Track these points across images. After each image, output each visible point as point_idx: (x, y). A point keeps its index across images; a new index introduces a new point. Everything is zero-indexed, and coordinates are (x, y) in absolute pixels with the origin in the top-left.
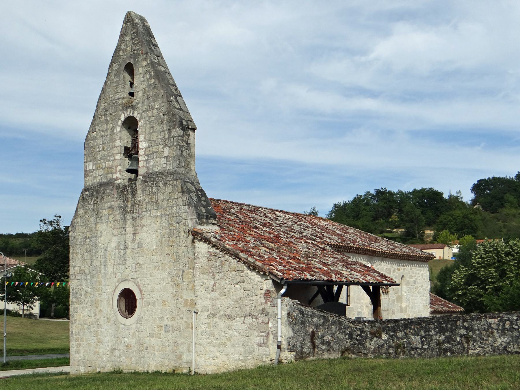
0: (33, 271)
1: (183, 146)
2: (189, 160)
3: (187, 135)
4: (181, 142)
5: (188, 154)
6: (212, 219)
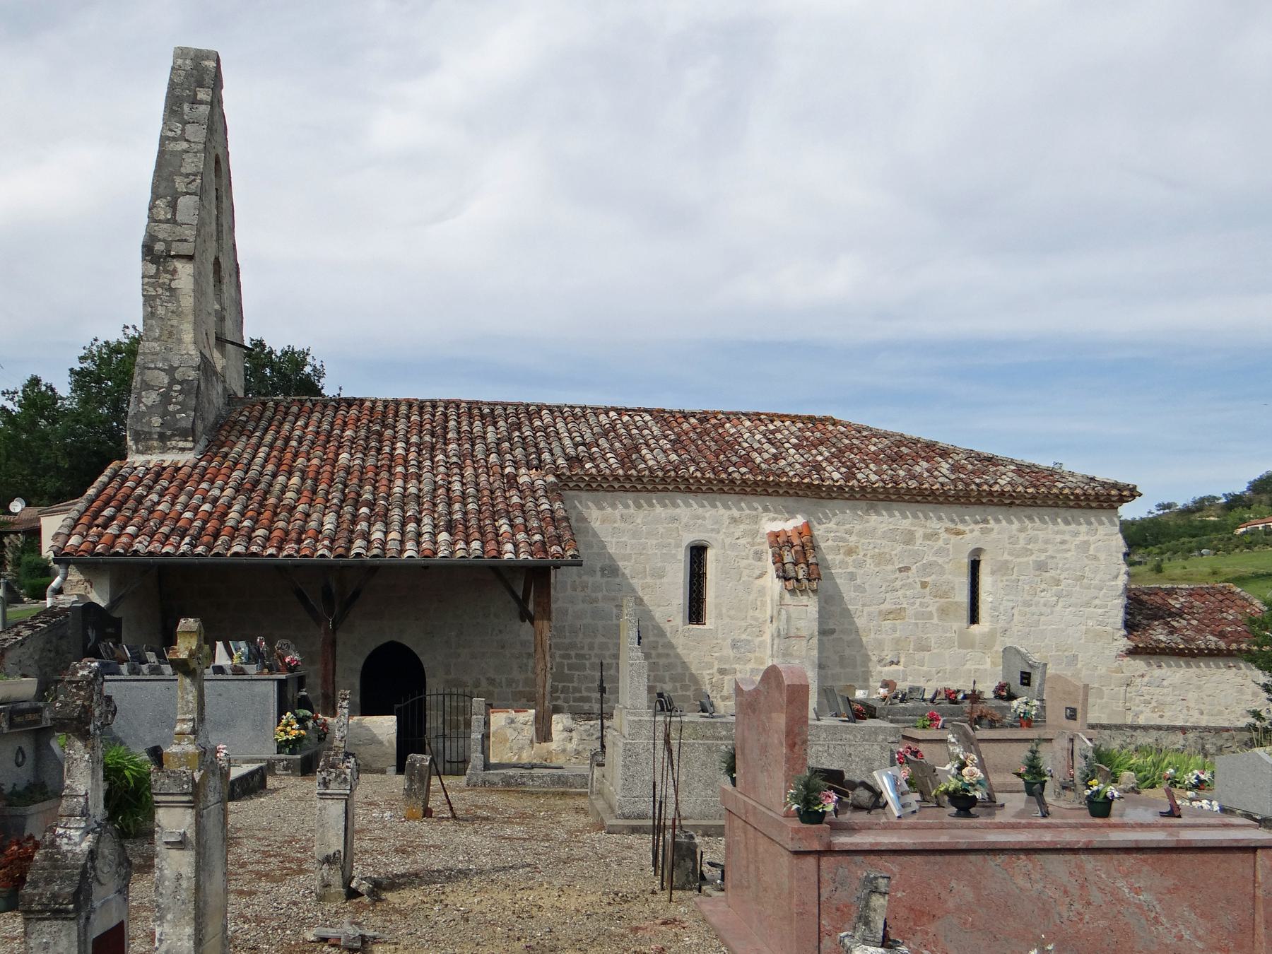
0: (1212, 518)
1: (157, 296)
2: (175, 323)
3: (167, 272)
4: (151, 289)
5: (173, 312)
6: (177, 438)
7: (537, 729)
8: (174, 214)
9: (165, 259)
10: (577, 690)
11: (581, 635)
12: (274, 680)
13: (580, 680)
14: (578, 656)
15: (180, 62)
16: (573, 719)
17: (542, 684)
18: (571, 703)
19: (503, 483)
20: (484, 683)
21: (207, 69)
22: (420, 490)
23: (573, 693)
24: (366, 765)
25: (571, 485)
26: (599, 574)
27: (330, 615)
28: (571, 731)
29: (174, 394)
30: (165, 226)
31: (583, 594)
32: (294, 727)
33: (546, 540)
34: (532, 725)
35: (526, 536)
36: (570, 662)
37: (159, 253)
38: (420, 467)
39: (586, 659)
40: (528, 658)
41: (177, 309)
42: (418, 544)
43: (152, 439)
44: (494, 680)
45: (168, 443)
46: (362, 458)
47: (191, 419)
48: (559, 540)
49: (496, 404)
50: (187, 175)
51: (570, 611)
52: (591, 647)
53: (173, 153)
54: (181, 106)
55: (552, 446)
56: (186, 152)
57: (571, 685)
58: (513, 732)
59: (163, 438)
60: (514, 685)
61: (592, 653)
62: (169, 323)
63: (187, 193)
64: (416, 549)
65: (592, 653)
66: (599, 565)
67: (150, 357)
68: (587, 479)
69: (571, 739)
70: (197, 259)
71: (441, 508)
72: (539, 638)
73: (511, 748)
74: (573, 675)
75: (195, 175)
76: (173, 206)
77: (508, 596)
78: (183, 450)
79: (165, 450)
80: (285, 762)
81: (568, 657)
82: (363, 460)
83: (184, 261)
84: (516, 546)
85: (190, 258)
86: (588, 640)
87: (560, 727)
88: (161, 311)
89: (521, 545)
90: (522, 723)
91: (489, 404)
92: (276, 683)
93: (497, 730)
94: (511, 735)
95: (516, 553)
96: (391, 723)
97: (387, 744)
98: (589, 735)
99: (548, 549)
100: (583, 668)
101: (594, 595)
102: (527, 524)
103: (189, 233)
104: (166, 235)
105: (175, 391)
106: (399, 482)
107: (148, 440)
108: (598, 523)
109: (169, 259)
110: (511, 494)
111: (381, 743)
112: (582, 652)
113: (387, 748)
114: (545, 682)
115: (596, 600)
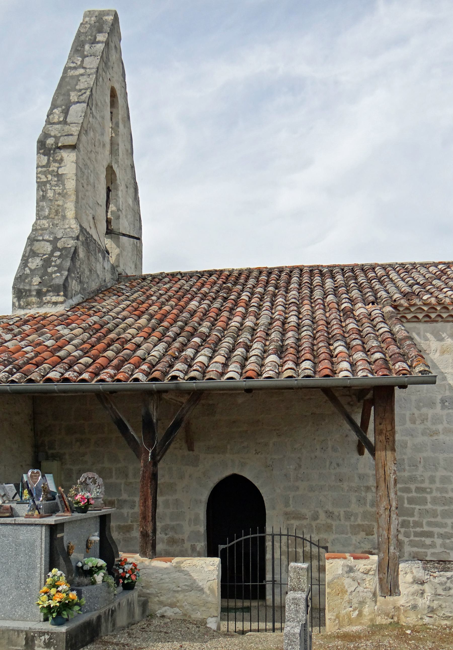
1: (48, 182)
2: (60, 203)
3: (55, 161)
5: (59, 194)
6: (51, 294)
7: (381, 580)
8: (66, 117)
9: (54, 151)
10: (417, 524)
11: (421, 469)
12: (42, 525)
13: (421, 514)
14: (419, 490)
15: (87, 19)
16: (425, 569)
17: (386, 526)
18: (412, 538)
19: (340, 316)
20: (322, 516)
21: (107, 21)
22: (256, 324)
23: (414, 527)
24: (185, 615)
25: (409, 316)
26: (439, 406)
27: (150, 446)
28: (423, 583)
29: (54, 259)
30: (57, 126)
31: (422, 426)
32: (60, 589)
33: (388, 359)
34: (374, 575)
35: (364, 355)
36: (410, 495)
37: (50, 146)
38: (260, 307)
39: (428, 493)
40: (366, 492)
41: (63, 191)
42: (243, 366)
43: (31, 296)
44: (332, 513)
45: (44, 298)
46: (209, 305)
47: (64, 277)
48: (404, 357)
49: (334, 266)
50: (80, 90)
51: (409, 444)
52: (432, 480)
53: (72, 77)
54: (83, 46)
55: (387, 288)
56: (82, 75)
57: (411, 519)
58: (352, 583)
59: (40, 294)
60: (352, 518)
61: (433, 486)
62: (56, 203)
63: (78, 102)
64: (240, 371)
65: (433, 486)
66: (439, 397)
67: (40, 232)
68: (426, 308)
69: (422, 594)
70: (82, 148)
71: (275, 336)
72: (381, 471)
73: (350, 602)
74: (414, 509)
75: (86, 89)
76: (66, 112)
77: (347, 426)
78: (55, 303)
79: (41, 304)
80: (47, 637)
81: (407, 490)
82: (209, 306)
83: (69, 150)
84: (353, 365)
85: (73, 147)
86: (429, 474)
87: (409, 578)
88: (50, 194)
89: (359, 363)
90: (363, 573)
91: (328, 267)
92: (44, 528)
93: (332, 580)
94: (350, 586)
95: (354, 372)
96: (212, 568)
97: (208, 592)
98: (445, 590)
99: (391, 367)
100: (424, 501)
101: (434, 428)
102: (365, 346)
103: (75, 130)
104: (57, 132)
105: (56, 257)
106: (238, 319)
107: (28, 296)
108: (438, 354)
109: (57, 150)
110: (347, 322)
111: (201, 590)
112: (423, 485)
113: (208, 596)
114: (389, 523)
115: (437, 433)
